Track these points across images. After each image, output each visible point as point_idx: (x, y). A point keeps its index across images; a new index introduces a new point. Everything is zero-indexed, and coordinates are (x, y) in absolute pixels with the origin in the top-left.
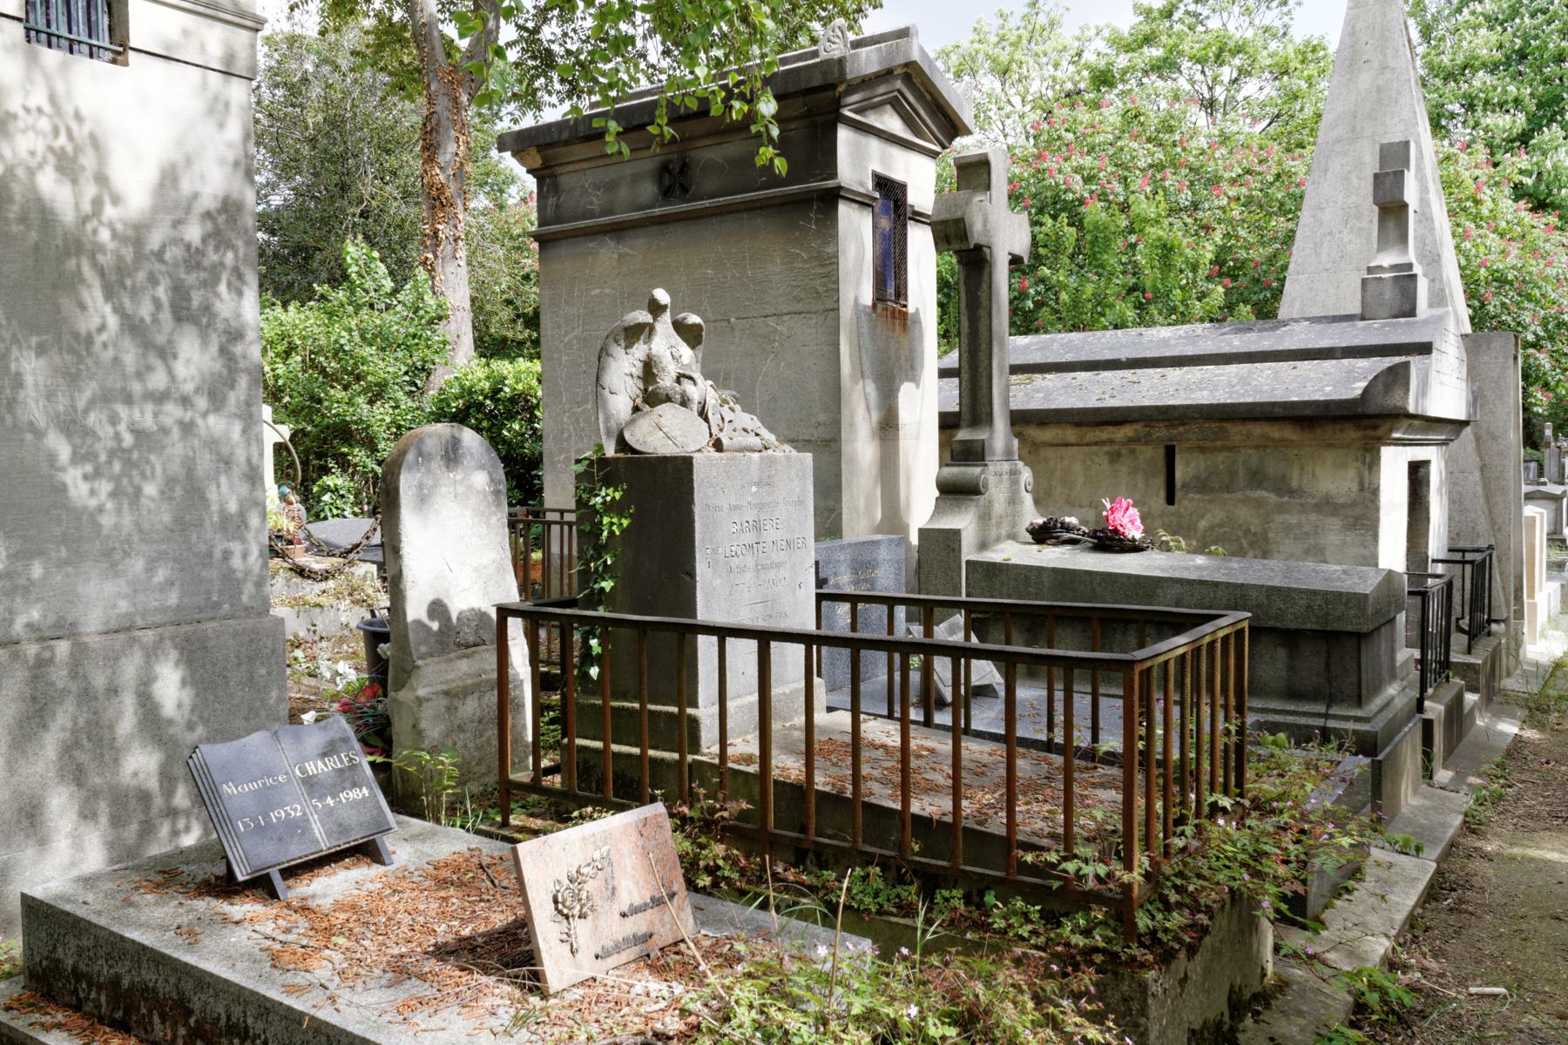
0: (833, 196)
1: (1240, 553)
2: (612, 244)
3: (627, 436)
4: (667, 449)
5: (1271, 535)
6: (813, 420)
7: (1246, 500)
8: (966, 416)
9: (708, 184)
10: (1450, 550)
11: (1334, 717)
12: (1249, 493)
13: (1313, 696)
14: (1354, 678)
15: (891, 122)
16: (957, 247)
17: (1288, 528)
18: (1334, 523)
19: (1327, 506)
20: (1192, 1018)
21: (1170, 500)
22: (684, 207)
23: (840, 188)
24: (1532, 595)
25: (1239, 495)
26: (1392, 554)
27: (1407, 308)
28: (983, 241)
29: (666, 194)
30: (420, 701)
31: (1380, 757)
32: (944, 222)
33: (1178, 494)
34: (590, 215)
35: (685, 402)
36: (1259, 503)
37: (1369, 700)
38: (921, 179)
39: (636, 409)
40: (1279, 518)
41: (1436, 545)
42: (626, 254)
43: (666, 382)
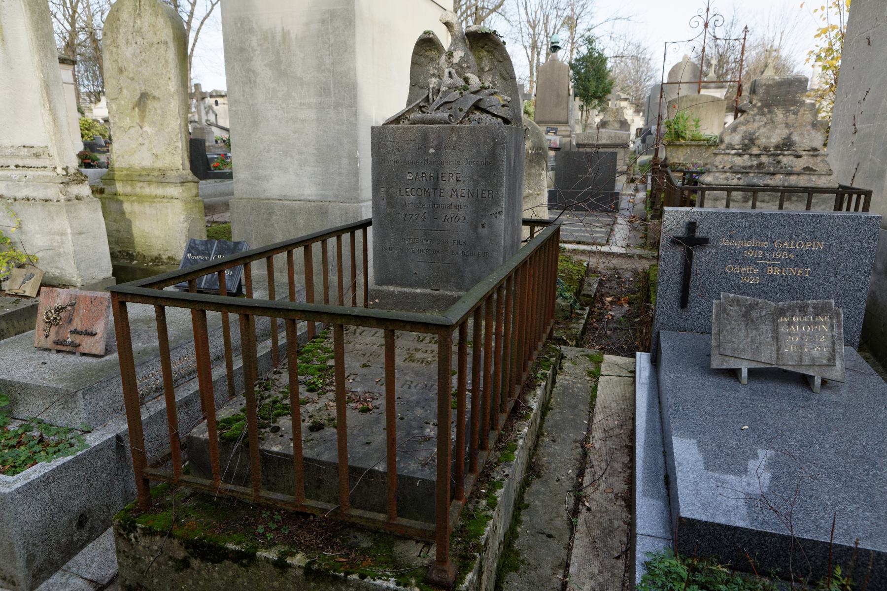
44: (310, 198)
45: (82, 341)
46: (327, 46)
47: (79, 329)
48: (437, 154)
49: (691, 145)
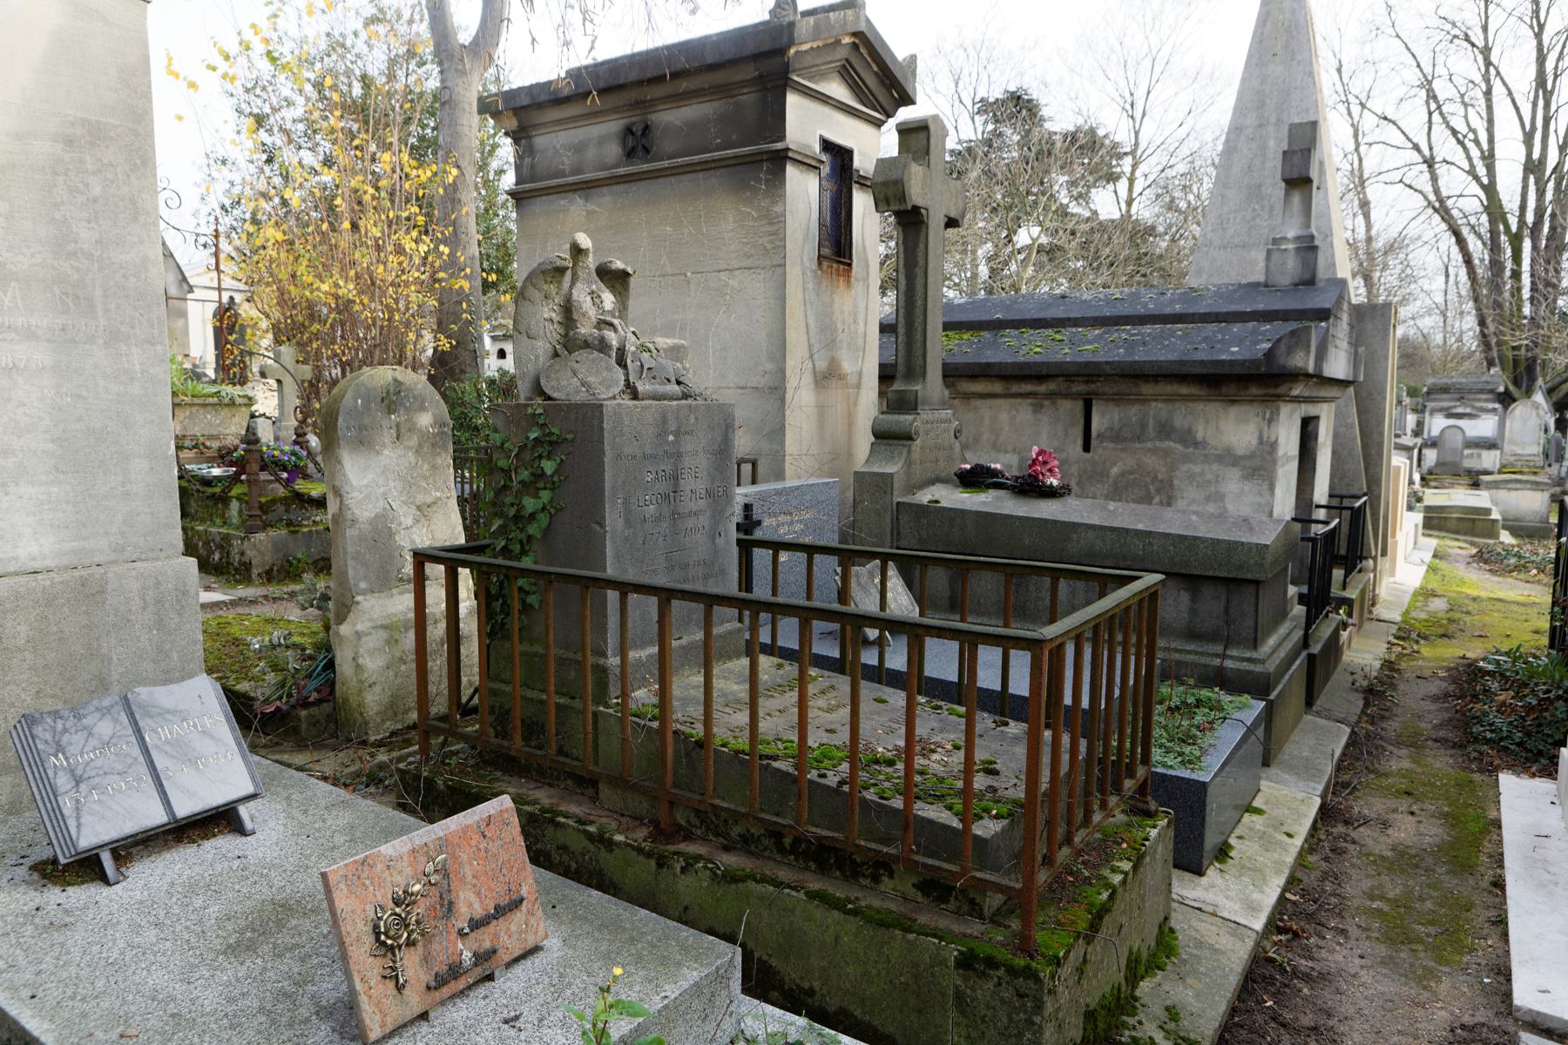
0: (781, 158)
1: (1147, 499)
2: (580, 201)
3: (543, 382)
4: (582, 396)
5: (1176, 482)
6: (761, 368)
7: (1154, 451)
8: (901, 368)
9: (668, 146)
10: (1331, 496)
11: (1232, 657)
12: (1157, 443)
13: (1213, 637)
14: (1251, 623)
15: (837, 89)
16: (896, 208)
17: (1191, 477)
18: (1235, 473)
19: (1229, 458)
20: (1088, 1000)
21: (1087, 447)
22: (645, 167)
23: (788, 149)
24: (1394, 536)
25: (1149, 445)
26: (1284, 503)
27: (1307, 276)
28: (919, 202)
29: (630, 154)
30: (358, 635)
31: (1272, 697)
32: (885, 184)
33: (1094, 443)
34: (562, 174)
35: (603, 346)
36: (1166, 453)
37: (1264, 640)
38: (875, 145)
39: (556, 355)
40: (1185, 467)
41: (1321, 493)
42: (593, 212)
43: (585, 329)
44: (37, 565)
45: (497, 936)
46: (80, 199)
47: (479, 912)
48: (676, 442)
49: (192, 405)
